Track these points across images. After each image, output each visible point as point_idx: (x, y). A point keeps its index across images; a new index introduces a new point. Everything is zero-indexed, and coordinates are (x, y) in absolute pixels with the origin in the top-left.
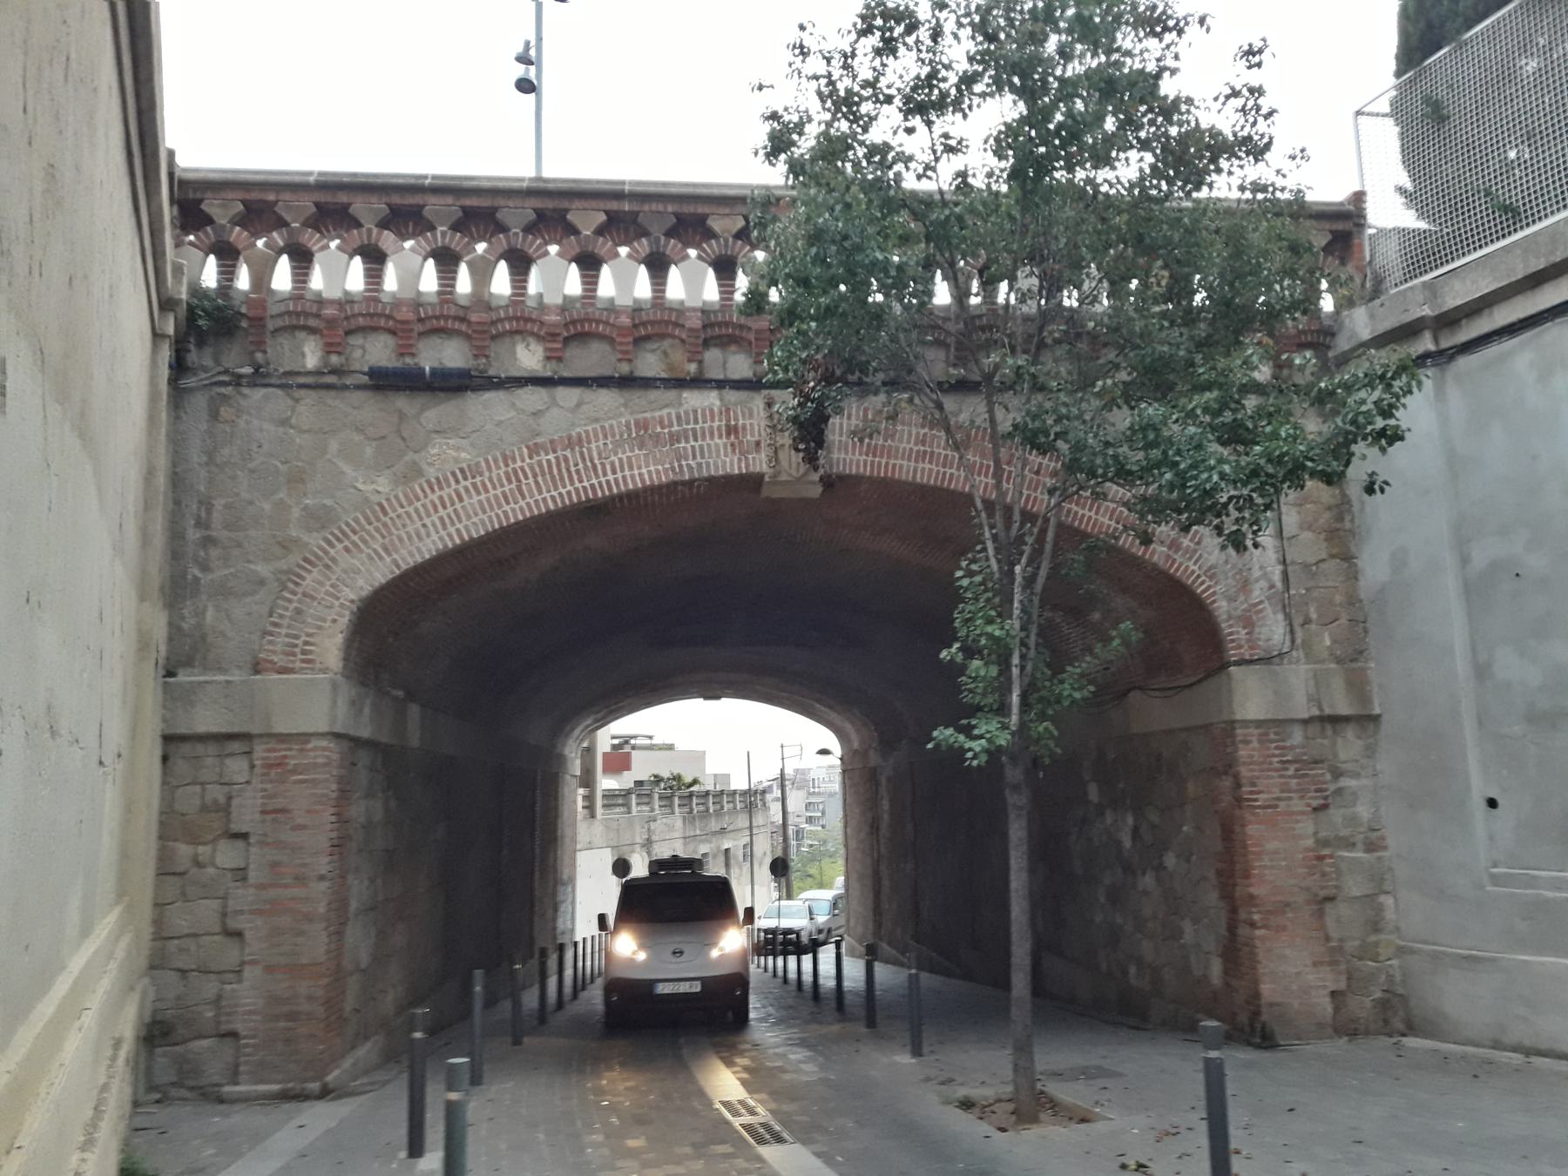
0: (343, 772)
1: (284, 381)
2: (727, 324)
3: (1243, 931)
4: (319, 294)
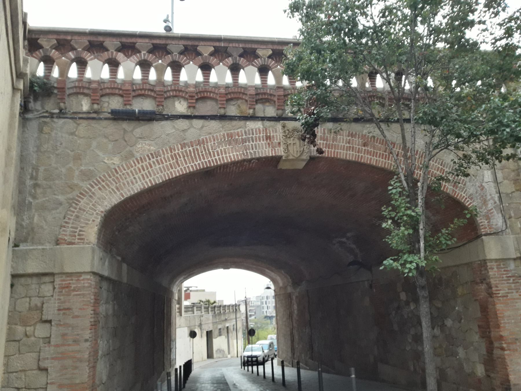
2: (265, 94)
3: (497, 352)
4: (89, 79)
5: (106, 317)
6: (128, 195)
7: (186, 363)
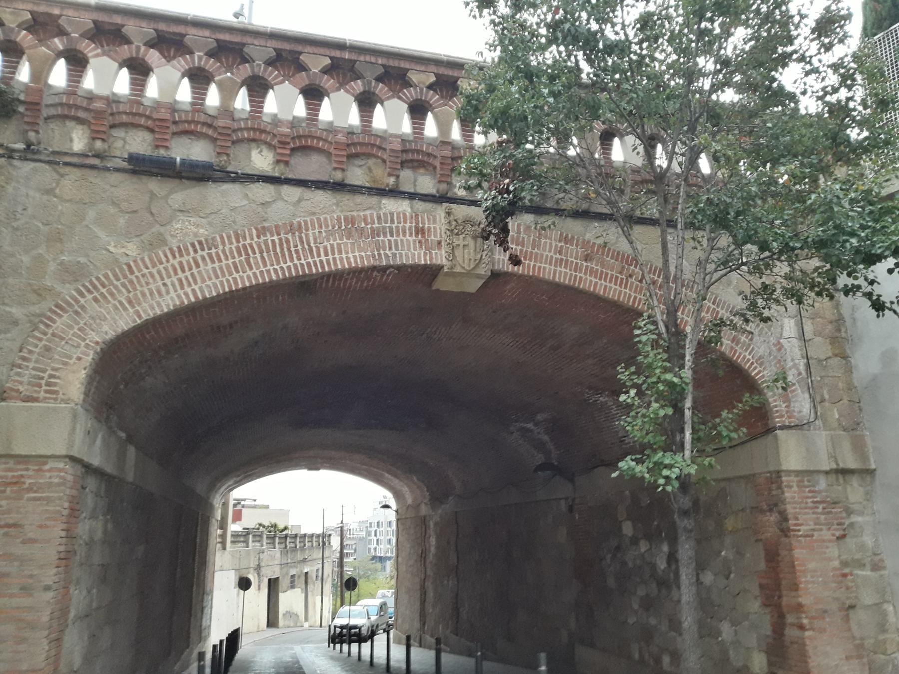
0: (74, 492)
1: (52, 159)
2: (418, 152)
3: (791, 633)
4: (90, 92)
5: (90, 543)
6: (149, 315)
7: (229, 634)
